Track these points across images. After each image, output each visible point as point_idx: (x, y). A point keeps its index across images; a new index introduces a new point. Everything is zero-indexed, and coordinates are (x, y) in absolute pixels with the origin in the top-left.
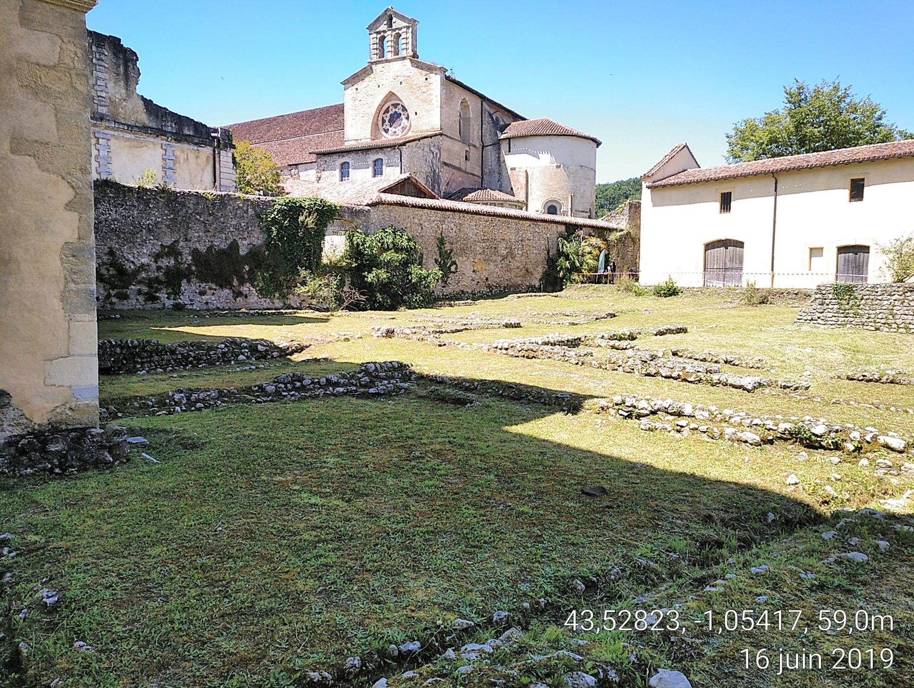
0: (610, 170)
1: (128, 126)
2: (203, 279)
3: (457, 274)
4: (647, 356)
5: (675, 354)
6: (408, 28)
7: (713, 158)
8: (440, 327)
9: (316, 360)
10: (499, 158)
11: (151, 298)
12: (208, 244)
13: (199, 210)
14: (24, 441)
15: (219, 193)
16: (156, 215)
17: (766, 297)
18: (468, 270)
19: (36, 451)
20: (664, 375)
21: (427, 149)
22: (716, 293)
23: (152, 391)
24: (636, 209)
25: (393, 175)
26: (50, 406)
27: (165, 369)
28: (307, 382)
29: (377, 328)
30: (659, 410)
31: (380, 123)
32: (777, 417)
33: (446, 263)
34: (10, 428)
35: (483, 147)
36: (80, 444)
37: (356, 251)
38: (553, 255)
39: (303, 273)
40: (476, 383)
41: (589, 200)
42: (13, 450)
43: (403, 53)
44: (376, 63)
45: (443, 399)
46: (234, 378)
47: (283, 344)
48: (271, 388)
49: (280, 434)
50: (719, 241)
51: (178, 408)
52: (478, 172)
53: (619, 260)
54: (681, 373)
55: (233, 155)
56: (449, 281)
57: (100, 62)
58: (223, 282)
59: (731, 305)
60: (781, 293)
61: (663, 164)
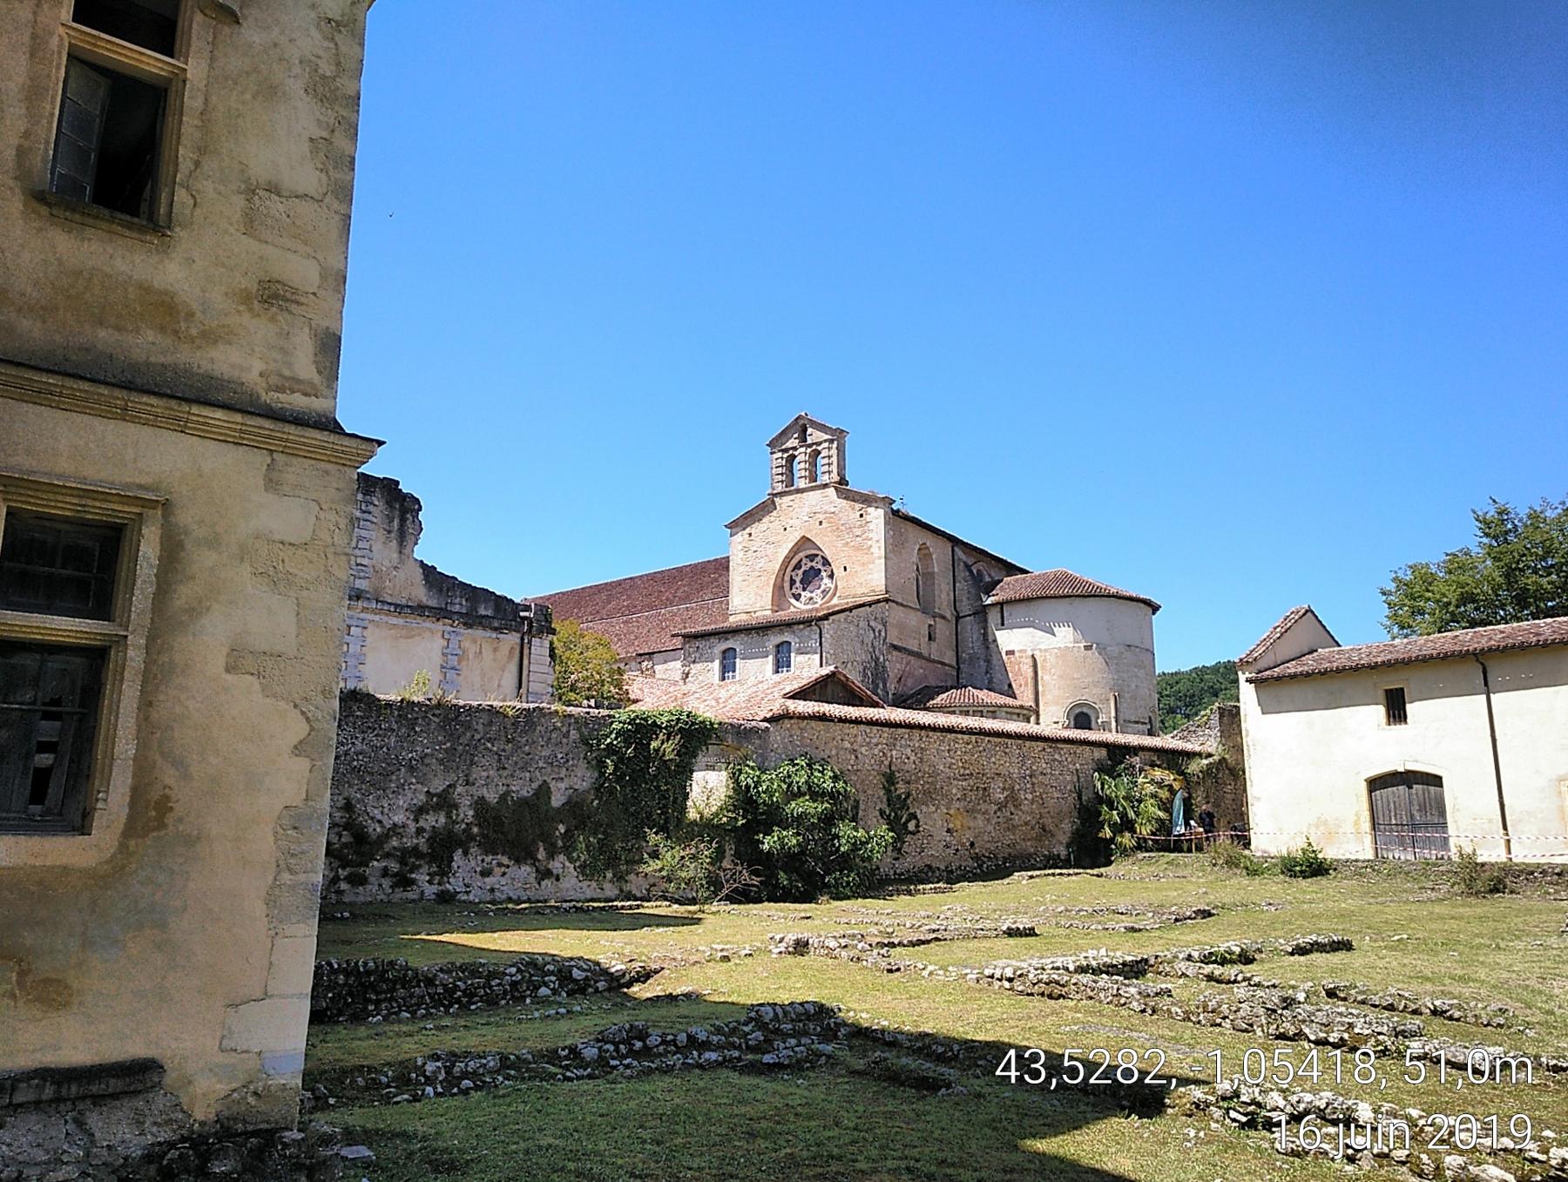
0: (1179, 649)
1: (396, 606)
2: (489, 848)
3: (919, 836)
4: (1275, 998)
5: (1331, 994)
6: (831, 441)
7: (1363, 631)
8: (890, 935)
9: (671, 998)
10: (985, 635)
11: (404, 882)
12: (502, 790)
13: (491, 735)
14: (173, 1154)
15: (525, 706)
16: (426, 743)
17: (1500, 881)
18: (938, 827)
19: (188, 1172)
20: (1312, 1038)
21: (863, 624)
22: (1399, 870)
23: (387, 1055)
24: (1231, 719)
25: (807, 668)
26: (222, 1088)
27: (413, 1013)
28: (653, 1040)
29: (778, 937)
30: (1307, 1112)
31: (787, 585)
32: (1547, 1133)
33: (899, 815)
34: (154, 1129)
35: (958, 618)
36: (262, 1161)
37: (743, 798)
38: (1089, 801)
39: (653, 838)
40: (956, 1047)
41: (1147, 701)
42: (153, 1169)
43: (825, 479)
44: (781, 494)
45: (895, 1078)
46: (528, 1032)
47: (617, 967)
48: (590, 1053)
49: (602, 1145)
50: (1395, 774)
51: (429, 1089)
52: (949, 658)
53: (1212, 806)
54: (1346, 1036)
55: (551, 643)
56: (905, 848)
57: (366, 516)
58: (522, 854)
59: (1433, 895)
60: (1529, 874)
61: (1272, 643)
